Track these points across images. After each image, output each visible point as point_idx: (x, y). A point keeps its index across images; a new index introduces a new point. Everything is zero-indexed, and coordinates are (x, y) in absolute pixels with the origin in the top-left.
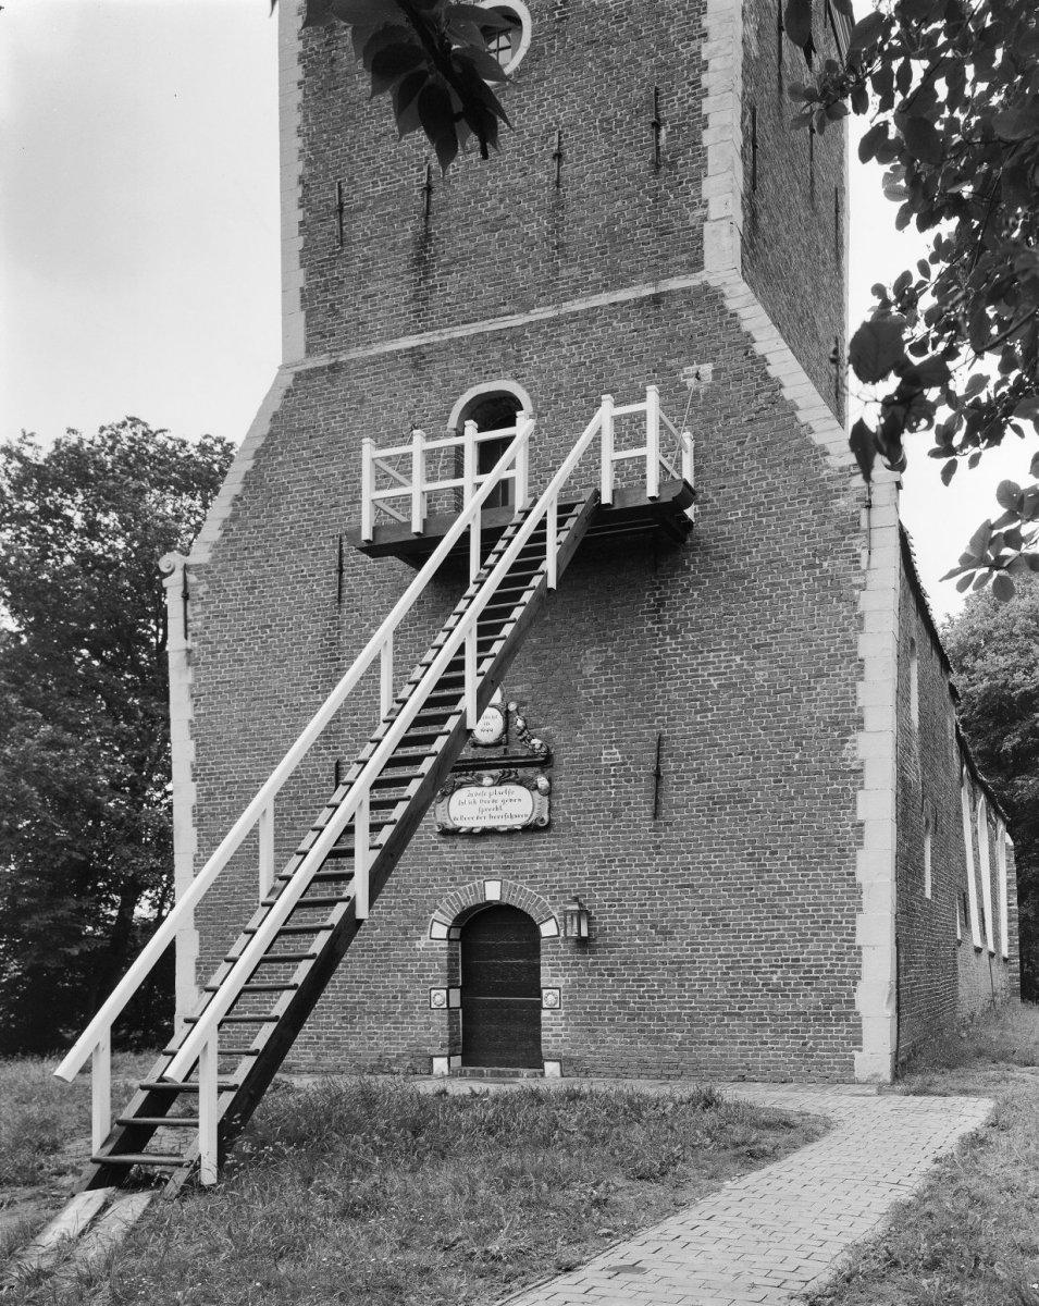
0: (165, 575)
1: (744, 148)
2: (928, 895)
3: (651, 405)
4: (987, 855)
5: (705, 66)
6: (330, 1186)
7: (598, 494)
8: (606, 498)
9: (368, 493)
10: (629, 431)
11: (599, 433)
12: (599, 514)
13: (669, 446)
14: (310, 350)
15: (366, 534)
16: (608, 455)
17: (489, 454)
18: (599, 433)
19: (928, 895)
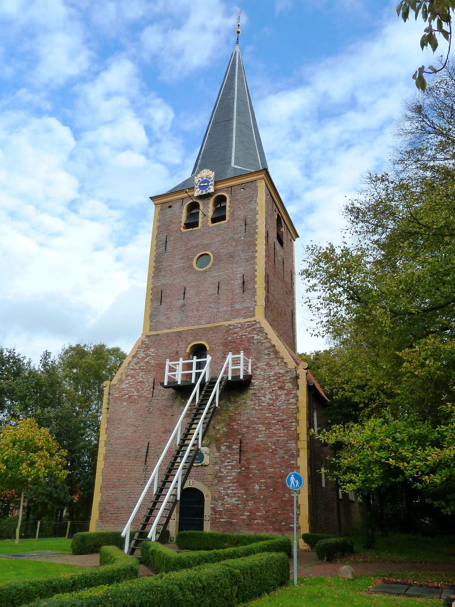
0: (105, 387)
1: (265, 288)
2: (324, 485)
3: (242, 355)
4: (175, 515)
5: (257, 240)
6: (415, 354)
7: (228, 377)
8: (230, 378)
9: (167, 373)
10: (236, 362)
11: (228, 363)
12: (228, 382)
13: (246, 365)
14: (151, 330)
15: (166, 384)
16: (231, 368)
17: (200, 366)
18: (228, 363)
19: (324, 485)
